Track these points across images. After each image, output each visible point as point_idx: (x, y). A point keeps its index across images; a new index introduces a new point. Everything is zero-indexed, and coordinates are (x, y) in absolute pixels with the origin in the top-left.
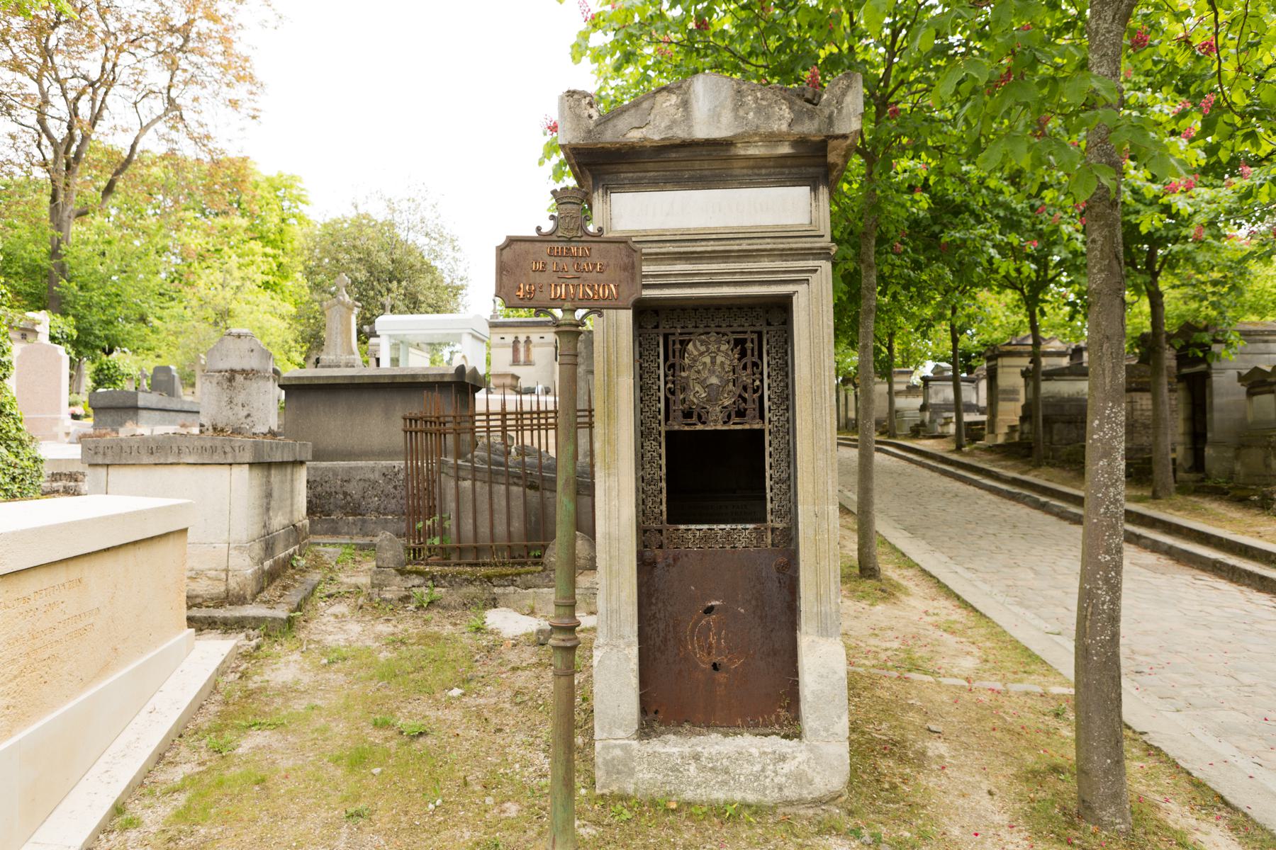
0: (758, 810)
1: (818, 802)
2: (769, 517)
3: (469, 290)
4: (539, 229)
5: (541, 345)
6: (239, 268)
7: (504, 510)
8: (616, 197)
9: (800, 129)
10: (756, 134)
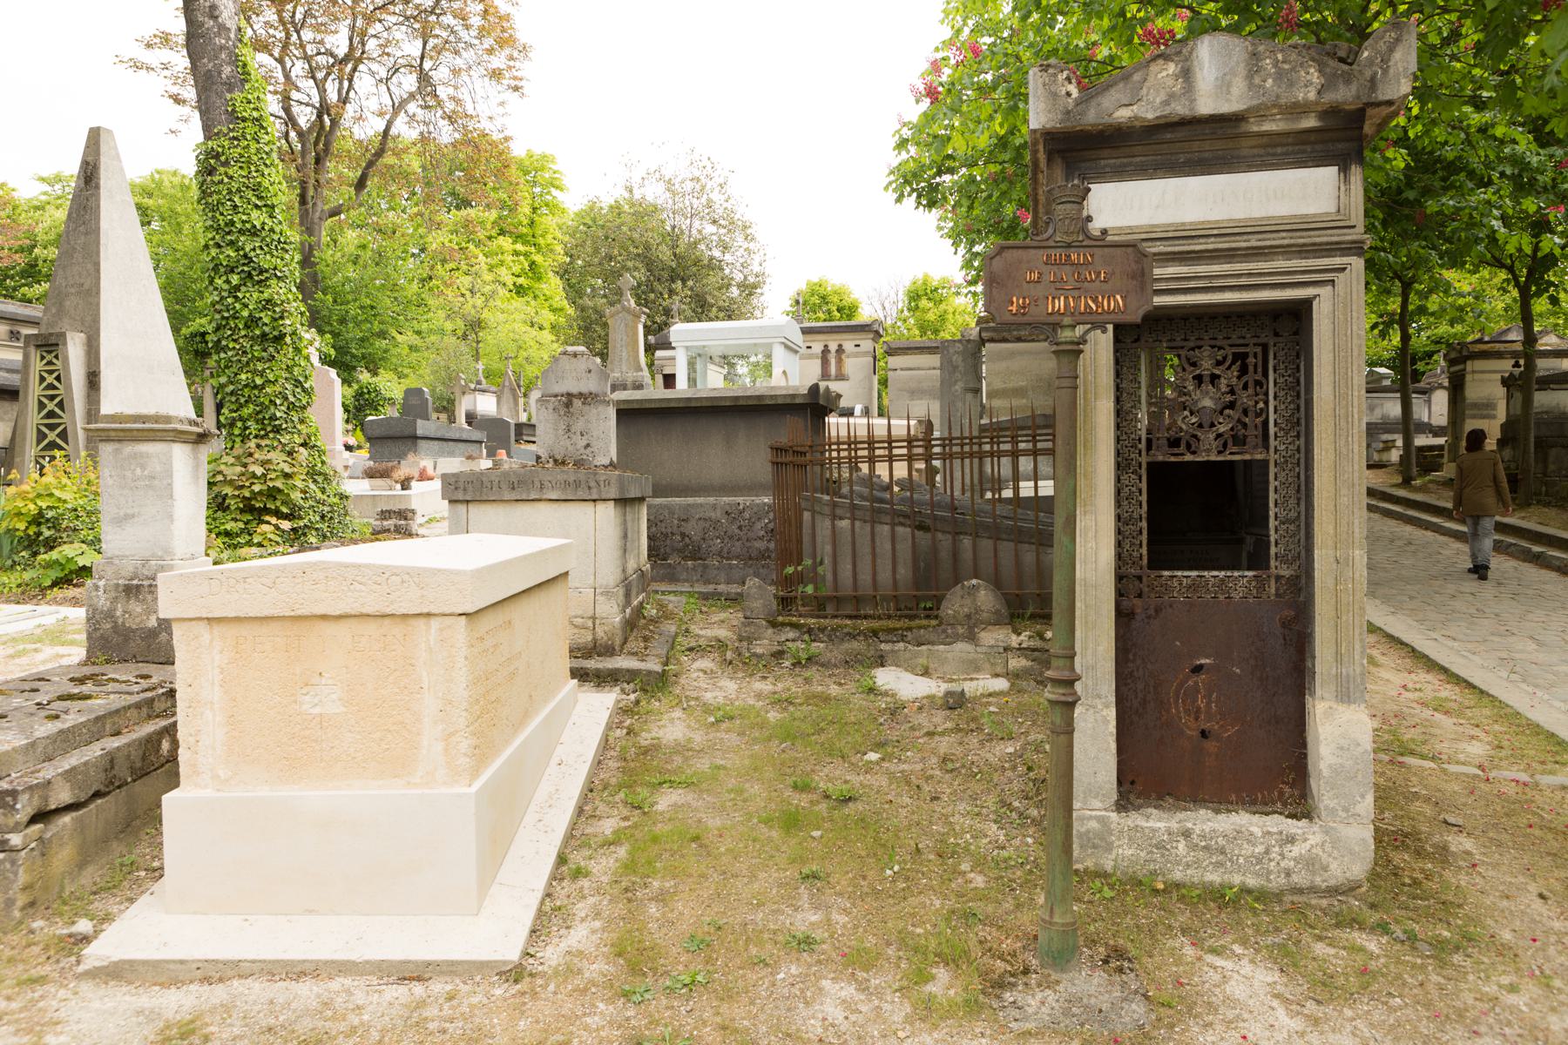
0: (1262, 896)
1: (1333, 891)
2: (1273, 563)
3: (766, 288)
5: (856, 355)
6: (490, 270)
7: (889, 554)
9: (1331, 97)
10: (1274, 106)
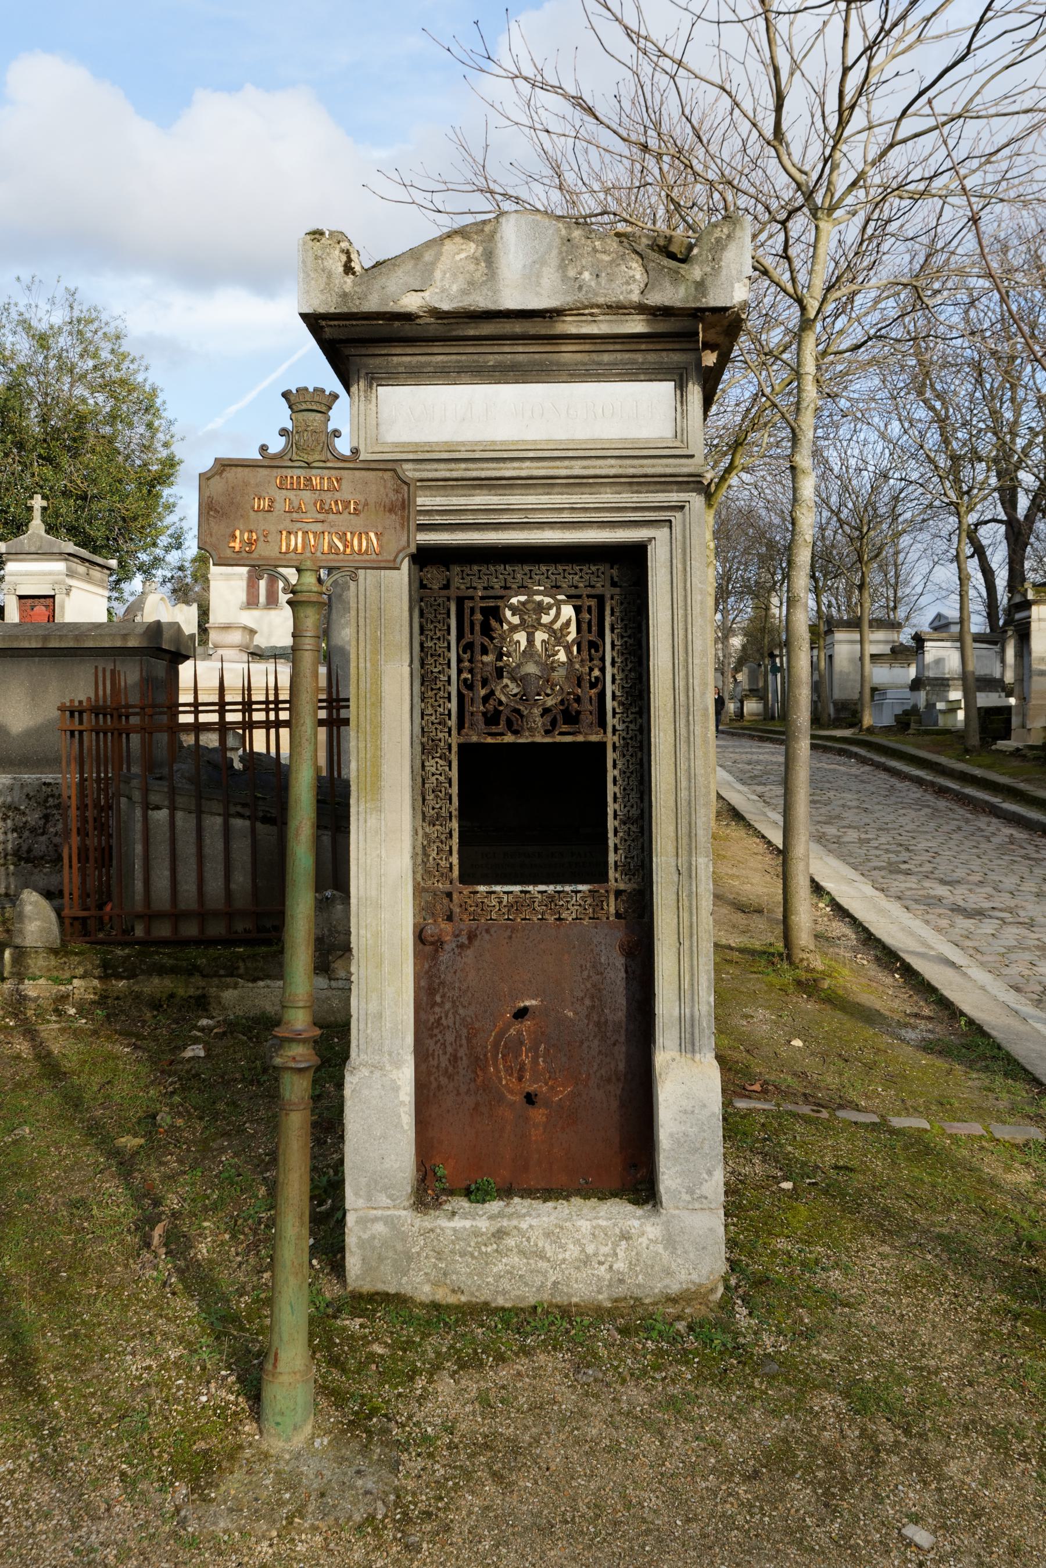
2: (612, 874)
4: (263, 448)
7: (221, 857)
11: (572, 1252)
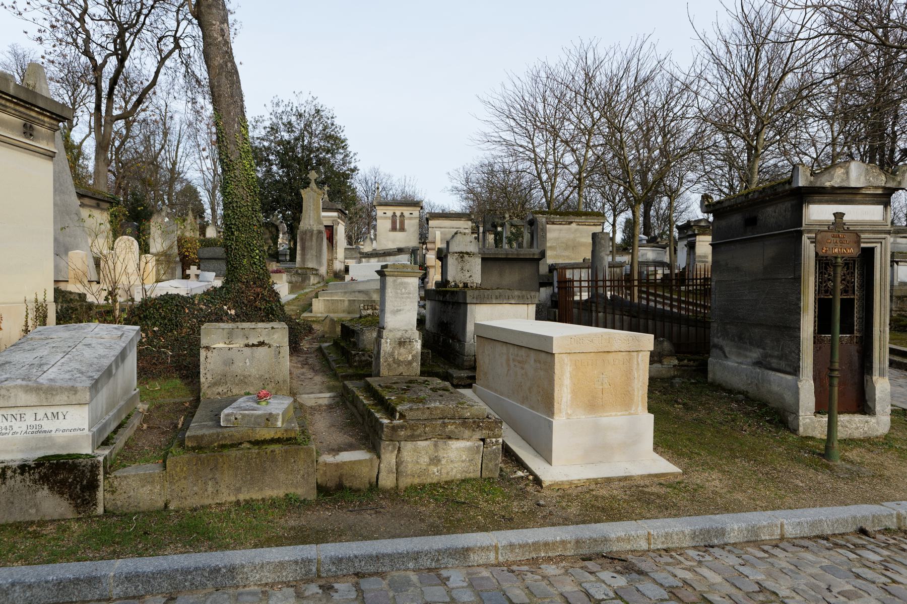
5: (410, 218)
8: (811, 206)
11: (854, 426)
